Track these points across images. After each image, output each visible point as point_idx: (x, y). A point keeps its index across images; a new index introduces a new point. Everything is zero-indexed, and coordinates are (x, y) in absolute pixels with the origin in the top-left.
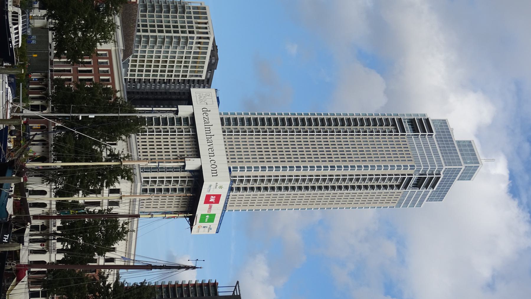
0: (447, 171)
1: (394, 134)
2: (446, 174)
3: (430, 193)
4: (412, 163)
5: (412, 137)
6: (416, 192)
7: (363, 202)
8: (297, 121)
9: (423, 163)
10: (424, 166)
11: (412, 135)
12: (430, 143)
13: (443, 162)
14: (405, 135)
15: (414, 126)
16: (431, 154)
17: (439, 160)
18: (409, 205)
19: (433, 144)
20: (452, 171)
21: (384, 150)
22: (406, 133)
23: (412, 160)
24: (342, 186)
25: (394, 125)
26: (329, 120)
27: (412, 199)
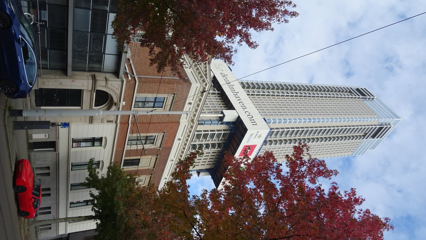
7: (203, 163)
24: (209, 144)
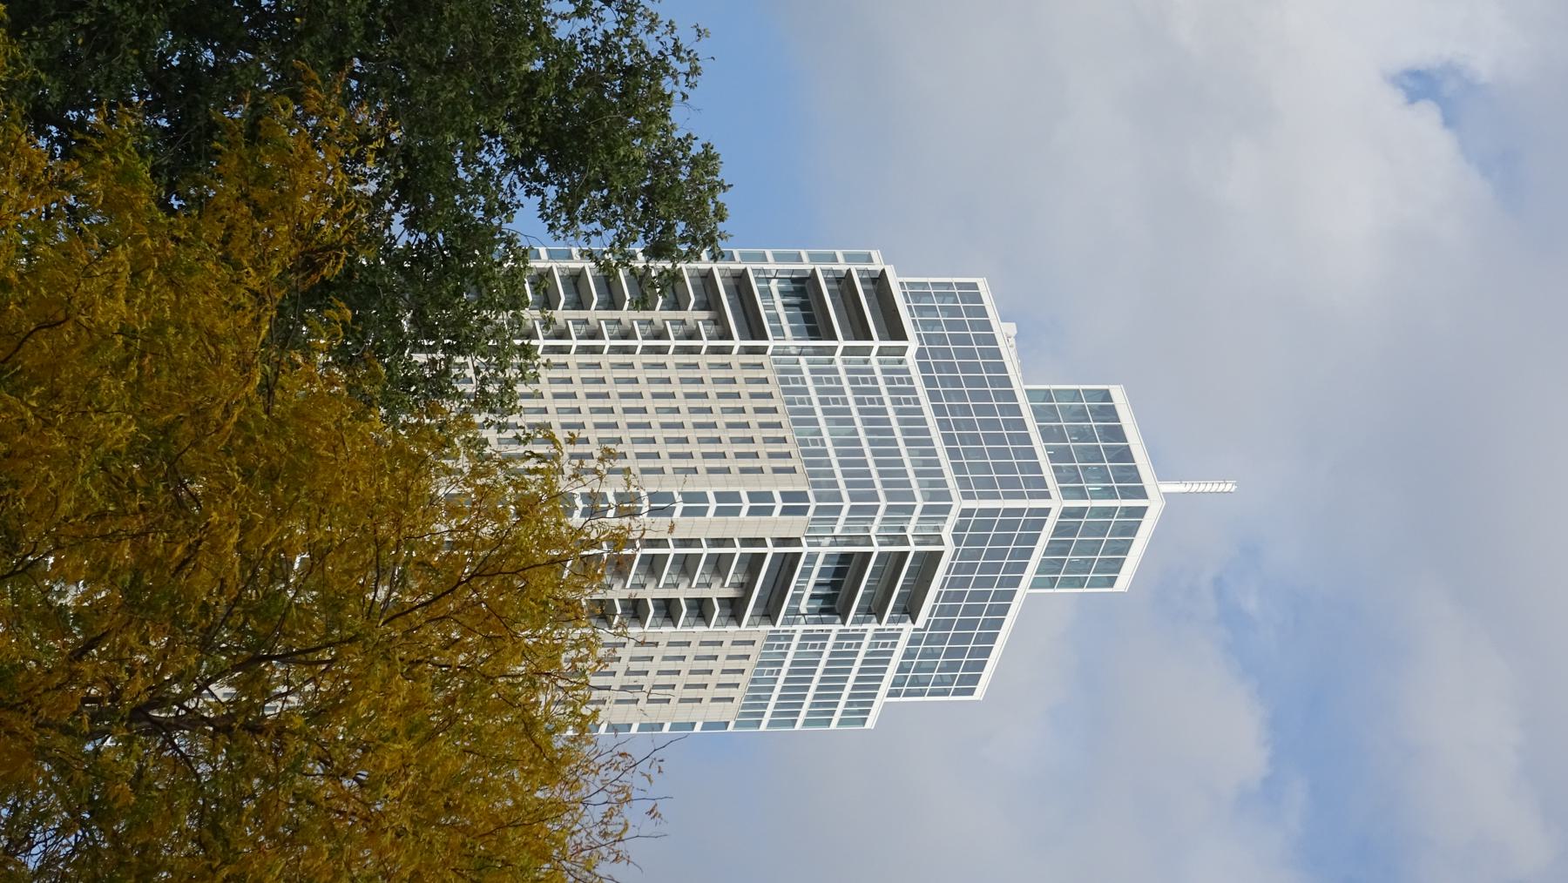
1: (705, 343)
2: (972, 540)
3: (902, 644)
4: (798, 484)
5: (802, 359)
6: (833, 637)
9: (848, 484)
10: (889, 496)
11: (802, 352)
14: (762, 351)
15: (816, 311)
16: (895, 442)
17: (928, 469)
18: (804, 711)
19: (902, 391)
21: (655, 420)
22: (766, 338)
23: (793, 470)
25: (709, 301)
26: (575, 284)
27: (817, 677)
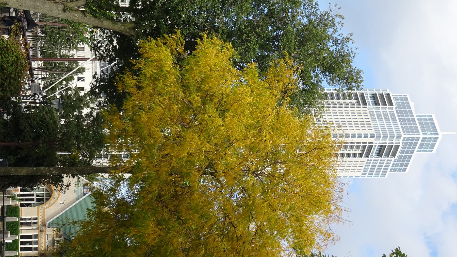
0: (407, 140)
3: (392, 162)
4: (373, 132)
8: (345, 95)
10: (390, 135)
12: (390, 115)
13: (401, 131)
15: (376, 100)
17: (397, 130)
20: (411, 140)
23: (372, 130)
25: (356, 98)
